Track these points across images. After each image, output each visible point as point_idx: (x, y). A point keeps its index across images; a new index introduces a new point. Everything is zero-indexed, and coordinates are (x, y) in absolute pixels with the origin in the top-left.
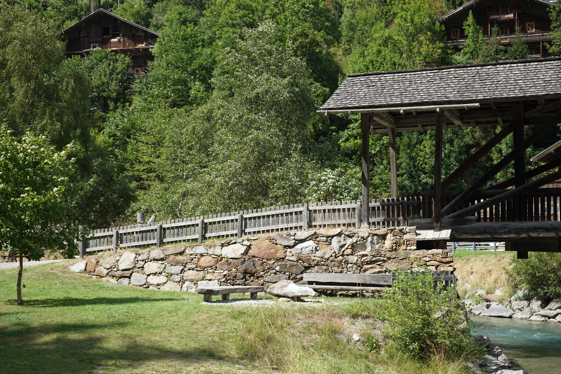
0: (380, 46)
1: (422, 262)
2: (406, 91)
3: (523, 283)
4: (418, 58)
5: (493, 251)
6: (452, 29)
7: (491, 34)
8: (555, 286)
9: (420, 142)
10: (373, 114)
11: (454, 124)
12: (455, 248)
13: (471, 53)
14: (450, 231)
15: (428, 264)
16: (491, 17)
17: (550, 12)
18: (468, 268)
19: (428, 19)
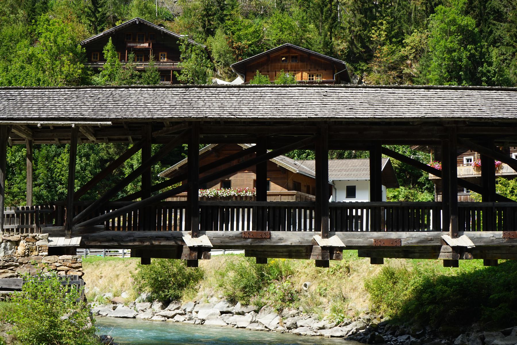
0: (23, 62)
1: (52, 267)
2: (44, 106)
3: (146, 286)
4: (59, 76)
5: (121, 257)
6: (93, 52)
7: (128, 60)
8: (174, 289)
9: (58, 155)
10: (11, 126)
11: (88, 139)
12: (87, 254)
13: (109, 75)
14: (80, 238)
15: (58, 269)
16: (129, 45)
17: (179, 45)
18: (97, 272)
19: (70, 41)
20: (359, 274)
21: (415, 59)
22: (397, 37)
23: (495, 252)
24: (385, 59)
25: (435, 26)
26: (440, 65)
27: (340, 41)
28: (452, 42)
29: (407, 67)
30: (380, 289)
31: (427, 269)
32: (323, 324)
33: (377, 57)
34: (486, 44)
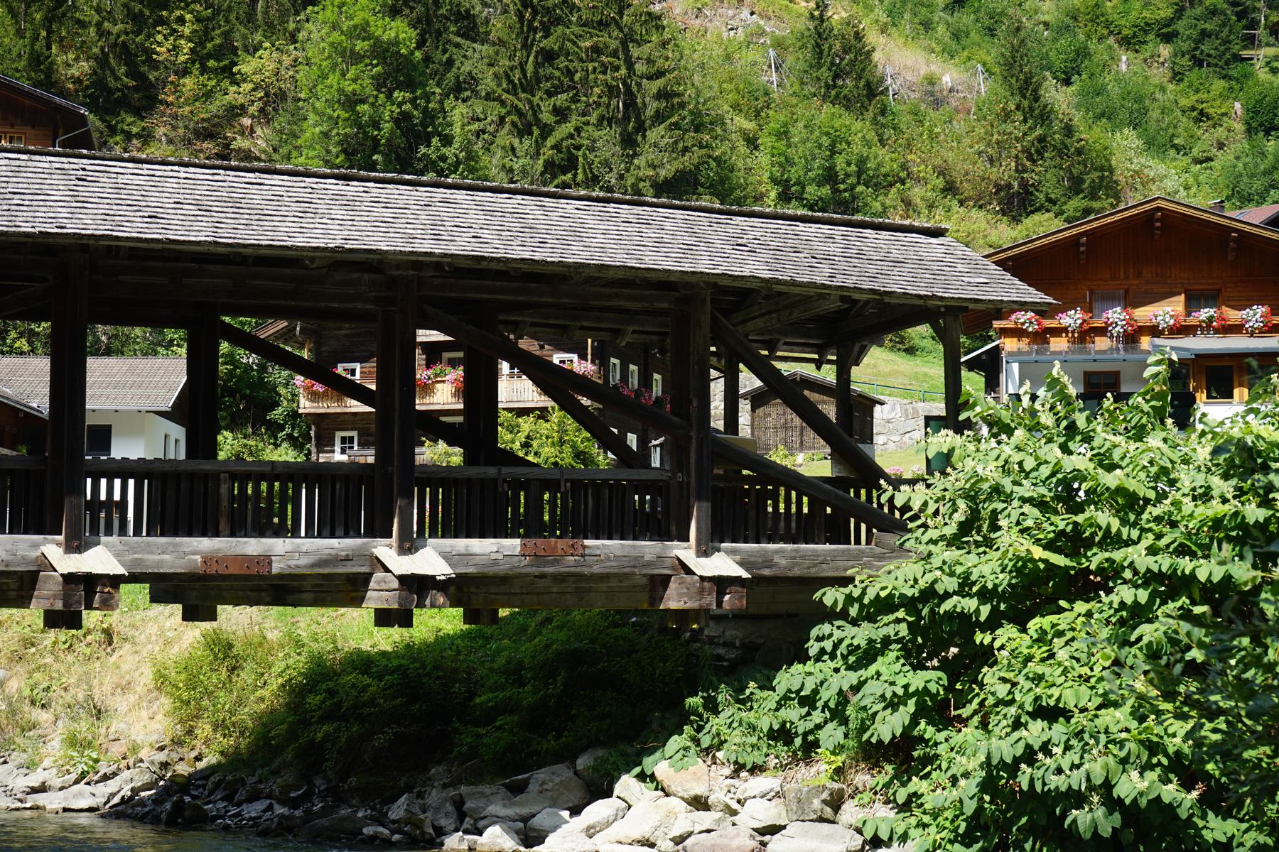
20: (138, 648)
21: (264, 116)
22: (218, 59)
23: (493, 589)
24: (188, 108)
25: (315, 36)
26: (326, 135)
27: (71, 56)
28: (360, 79)
29: (242, 133)
30: (192, 684)
31: (317, 634)
32: (41, 780)
33: (168, 104)
34: (438, 90)
